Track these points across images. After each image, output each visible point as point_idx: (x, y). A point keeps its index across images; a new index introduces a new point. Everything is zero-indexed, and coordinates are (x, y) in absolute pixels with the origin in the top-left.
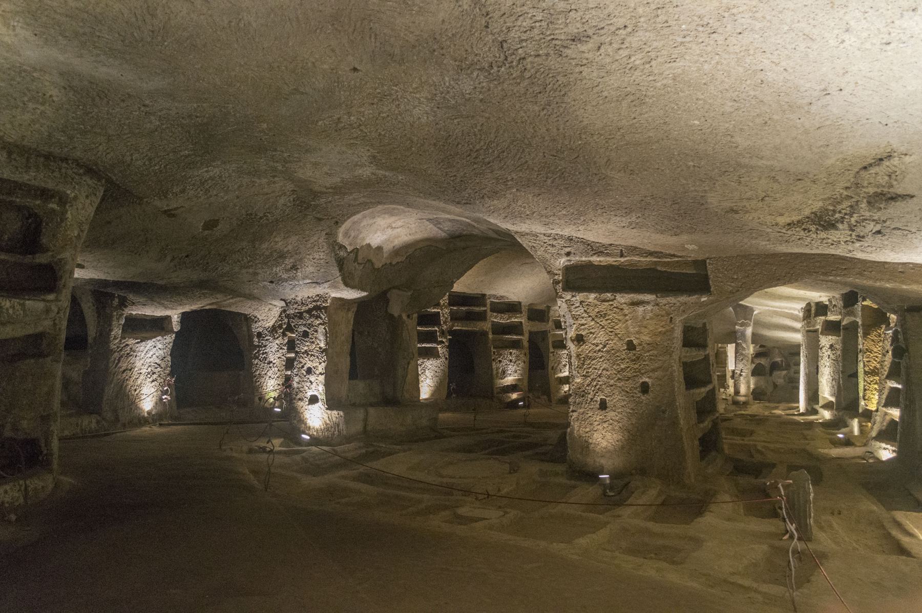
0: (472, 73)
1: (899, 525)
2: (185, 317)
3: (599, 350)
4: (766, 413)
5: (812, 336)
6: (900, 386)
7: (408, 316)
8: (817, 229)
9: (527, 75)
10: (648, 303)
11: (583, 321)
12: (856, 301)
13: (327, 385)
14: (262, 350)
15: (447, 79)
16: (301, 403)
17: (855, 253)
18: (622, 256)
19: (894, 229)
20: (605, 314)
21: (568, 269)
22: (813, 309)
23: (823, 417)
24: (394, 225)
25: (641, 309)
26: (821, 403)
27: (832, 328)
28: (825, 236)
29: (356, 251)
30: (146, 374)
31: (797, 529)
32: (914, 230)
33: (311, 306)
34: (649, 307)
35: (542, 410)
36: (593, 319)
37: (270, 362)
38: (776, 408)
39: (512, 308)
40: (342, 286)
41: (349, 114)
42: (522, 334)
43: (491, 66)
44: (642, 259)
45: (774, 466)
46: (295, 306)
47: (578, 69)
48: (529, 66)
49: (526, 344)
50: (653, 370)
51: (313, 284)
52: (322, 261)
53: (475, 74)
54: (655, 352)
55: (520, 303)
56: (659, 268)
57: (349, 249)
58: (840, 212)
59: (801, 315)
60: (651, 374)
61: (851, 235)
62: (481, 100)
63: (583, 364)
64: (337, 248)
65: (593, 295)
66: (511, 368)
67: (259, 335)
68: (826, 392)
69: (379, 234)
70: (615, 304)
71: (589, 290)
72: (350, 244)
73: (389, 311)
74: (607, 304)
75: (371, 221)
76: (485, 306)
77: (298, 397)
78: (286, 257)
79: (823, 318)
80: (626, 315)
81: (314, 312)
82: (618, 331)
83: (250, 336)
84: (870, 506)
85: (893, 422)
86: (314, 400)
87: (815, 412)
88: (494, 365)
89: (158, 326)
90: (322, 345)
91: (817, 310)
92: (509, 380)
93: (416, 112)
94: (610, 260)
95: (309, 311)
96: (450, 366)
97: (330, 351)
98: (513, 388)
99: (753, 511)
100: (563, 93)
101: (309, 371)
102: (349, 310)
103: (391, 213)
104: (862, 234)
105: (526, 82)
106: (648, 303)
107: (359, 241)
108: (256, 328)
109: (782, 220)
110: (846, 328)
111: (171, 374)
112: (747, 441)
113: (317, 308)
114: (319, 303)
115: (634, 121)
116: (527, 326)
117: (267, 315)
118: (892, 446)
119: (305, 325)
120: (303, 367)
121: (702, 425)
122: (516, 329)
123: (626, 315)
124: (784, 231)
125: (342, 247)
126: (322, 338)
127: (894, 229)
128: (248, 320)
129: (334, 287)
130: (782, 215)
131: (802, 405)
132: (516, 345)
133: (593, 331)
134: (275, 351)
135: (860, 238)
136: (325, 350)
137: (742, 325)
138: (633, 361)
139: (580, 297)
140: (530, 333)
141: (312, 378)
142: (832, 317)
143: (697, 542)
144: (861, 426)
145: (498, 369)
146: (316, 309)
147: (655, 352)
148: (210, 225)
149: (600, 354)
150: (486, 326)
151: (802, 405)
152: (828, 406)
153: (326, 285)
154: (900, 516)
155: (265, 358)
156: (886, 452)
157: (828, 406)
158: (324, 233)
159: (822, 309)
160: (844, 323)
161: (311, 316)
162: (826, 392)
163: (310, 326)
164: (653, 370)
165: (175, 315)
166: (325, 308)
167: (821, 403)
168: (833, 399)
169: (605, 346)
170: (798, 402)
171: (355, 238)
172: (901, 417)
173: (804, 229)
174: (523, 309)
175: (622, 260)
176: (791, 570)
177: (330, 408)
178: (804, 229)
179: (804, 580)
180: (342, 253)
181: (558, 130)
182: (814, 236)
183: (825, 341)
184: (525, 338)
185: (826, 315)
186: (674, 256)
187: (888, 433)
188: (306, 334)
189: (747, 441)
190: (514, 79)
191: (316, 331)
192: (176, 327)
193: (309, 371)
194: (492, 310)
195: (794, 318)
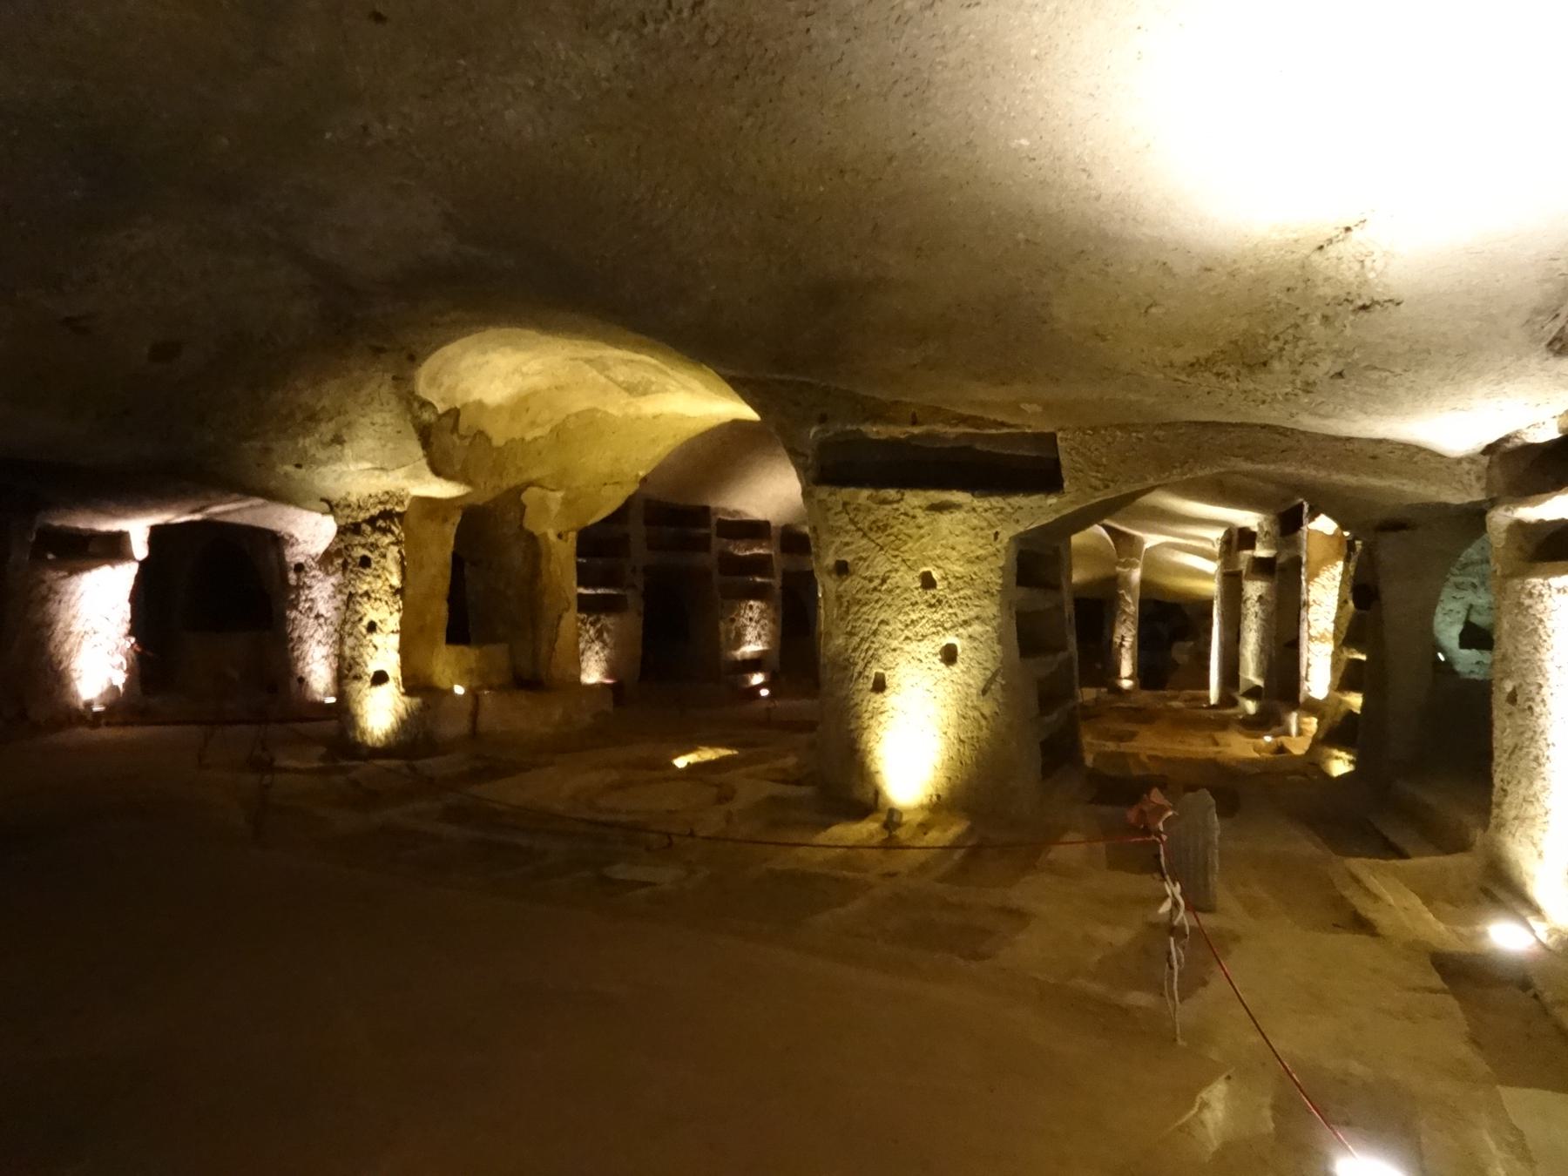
0: (607, 34)
1: (1356, 880)
2: (158, 535)
3: (875, 589)
4: (1160, 706)
5: (1232, 583)
6: (1363, 657)
7: (560, 536)
8: (1239, 373)
9: (711, 38)
10: (958, 506)
11: (847, 539)
12: (1298, 524)
13: (404, 650)
14: (304, 594)
15: (560, 45)
16: (357, 685)
17: (1299, 418)
18: (914, 423)
19: (1367, 368)
20: (886, 526)
21: (824, 447)
22: (1235, 538)
23: (1245, 711)
24: (525, 369)
25: (945, 520)
26: (1243, 688)
27: (1263, 568)
28: (1252, 386)
29: (454, 414)
30: (95, 630)
31: (1183, 894)
32: (1398, 370)
33: (375, 512)
34: (959, 515)
35: (795, 703)
36: (865, 535)
37: (318, 616)
38: (1175, 698)
39: (756, 530)
40: (429, 475)
41: (384, 121)
42: (771, 576)
43: (643, 21)
44: (948, 429)
45: (1537, 911)
46: (347, 511)
47: (802, 23)
48: (711, 19)
49: (778, 591)
50: (966, 623)
51: (374, 469)
52: (389, 429)
53: (614, 37)
54: (969, 592)
55: (767, 523)
56: (978, 446)
57: (441, 408)
58: (1276, 338)
59: (1217, 549)
60: (961, 630)
61: (1293, 382)
62: (631, 95)
63: (847, 612)
64: (416, 405)
65: (865, 493)
66: (751, 633)
67: (299, 568)
68: (1251, 673)
69: (498, 383)
70: (903, 507)
71: (860, 483)
72: (443, 400)
73: (527, 525)
74: (888, 507)
75: (481, 360)
76: (707, 525)
77: (353, 673)
78: (320, 420)
79: (1248, 553)
80: (920, 527)
81: (381, 523)
82: (906, 556)
83: (283, 567)
84: (1306, 847)
85: (1351, 714)
86: (380, 678)
87: (1234, 703)
88: (722, 626)
89: (115, 548)
90: (396, 581)
91: (1240, 540)
92: (752, 647)
93: (510, 114)
94: (898, 432)
95: (372, 521)
96: (648, 627)
97: (409, 592)
98: (754, 664)
99: (1119, 862)
100: (778, 78)
101: (372, 627)
102: (445, 520)
103: (517, 347)
104: (1312, 379)
105: (709, 56)
106: (958, 506)
107: (459, 395)
108: (294, 555)
109: (1179, 356)
110: (1283, 569)
111: (131, 633)
112: (1126, 747)
113: (387, 515)
114: (388, 507)
115: (913, 141)
116: (780, 563)
117: (311, 532)
118: (1348, 753)
119: (364, 546)
120: (361, 619)
121: (1047, 719)
122: (760, 565)
123: (920, 527)
124: (1183, 377)
125: (425, 404)
126: (394, 568)
127: (1367, 368)
128: (276, 541)
129: (415, 476)
130: (1178, 345)
131: (1214, 694)
132: (758, 593)
133: (864, 555)
134: (322, 593)
135: (1308, 387)
136: (397, 592)
137: (1125, 565)
138: (931, 606)
139: (846, 493)
140: (786, 575)
141: (376, 638)
142: (1262, 552)
143: (1020, 917)
144: (1299, 724)
145: (728, 632)
146: (385, 518)
147: (969, 592)
148: (164, 352)
149: (876, 595)
150: (708, 560)
151: (1214, 694)
152: (1253, 693)
153: (401, 473)
154: (1358, 865)
155: (310, 609)
156: (1340, 765)
157: (1253, 693)
158: (388, 377)
159: (1244, 538)
160: (1281, 560)
161: (375, 529)
162: (1251, 673)
163: (374, 546)
164: (966, 623)
165: (138, 529)
166: (400, 515)
167: (1243, 688)
168: (1259, 682)
169: (884, 581)
170: (1206, 686)
171: (451, 389)
172: (1364, 707)
173: (1218, 374)
174: (773, 533)
175: (916, 430)
176: (1171, 967)
177: (409, 691)
178: (1218, 374)
179: (1193, 983)
180: (426, 416)
181: (779, 160)
182: (1233, 385)
183: (1254, 589)
184: (776, 582)
185: (1252, 547)
186: (1003, 424)
187: (1340, 732)
188: (365, 562)
189: (1126, 747)
190: (688, 46)
191: (384, 556)
192: (140, 550)
193: (372, 627)
194: (720, 534)
195: (1208, 556)
